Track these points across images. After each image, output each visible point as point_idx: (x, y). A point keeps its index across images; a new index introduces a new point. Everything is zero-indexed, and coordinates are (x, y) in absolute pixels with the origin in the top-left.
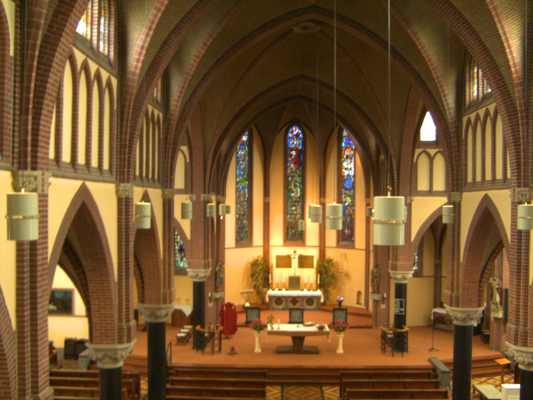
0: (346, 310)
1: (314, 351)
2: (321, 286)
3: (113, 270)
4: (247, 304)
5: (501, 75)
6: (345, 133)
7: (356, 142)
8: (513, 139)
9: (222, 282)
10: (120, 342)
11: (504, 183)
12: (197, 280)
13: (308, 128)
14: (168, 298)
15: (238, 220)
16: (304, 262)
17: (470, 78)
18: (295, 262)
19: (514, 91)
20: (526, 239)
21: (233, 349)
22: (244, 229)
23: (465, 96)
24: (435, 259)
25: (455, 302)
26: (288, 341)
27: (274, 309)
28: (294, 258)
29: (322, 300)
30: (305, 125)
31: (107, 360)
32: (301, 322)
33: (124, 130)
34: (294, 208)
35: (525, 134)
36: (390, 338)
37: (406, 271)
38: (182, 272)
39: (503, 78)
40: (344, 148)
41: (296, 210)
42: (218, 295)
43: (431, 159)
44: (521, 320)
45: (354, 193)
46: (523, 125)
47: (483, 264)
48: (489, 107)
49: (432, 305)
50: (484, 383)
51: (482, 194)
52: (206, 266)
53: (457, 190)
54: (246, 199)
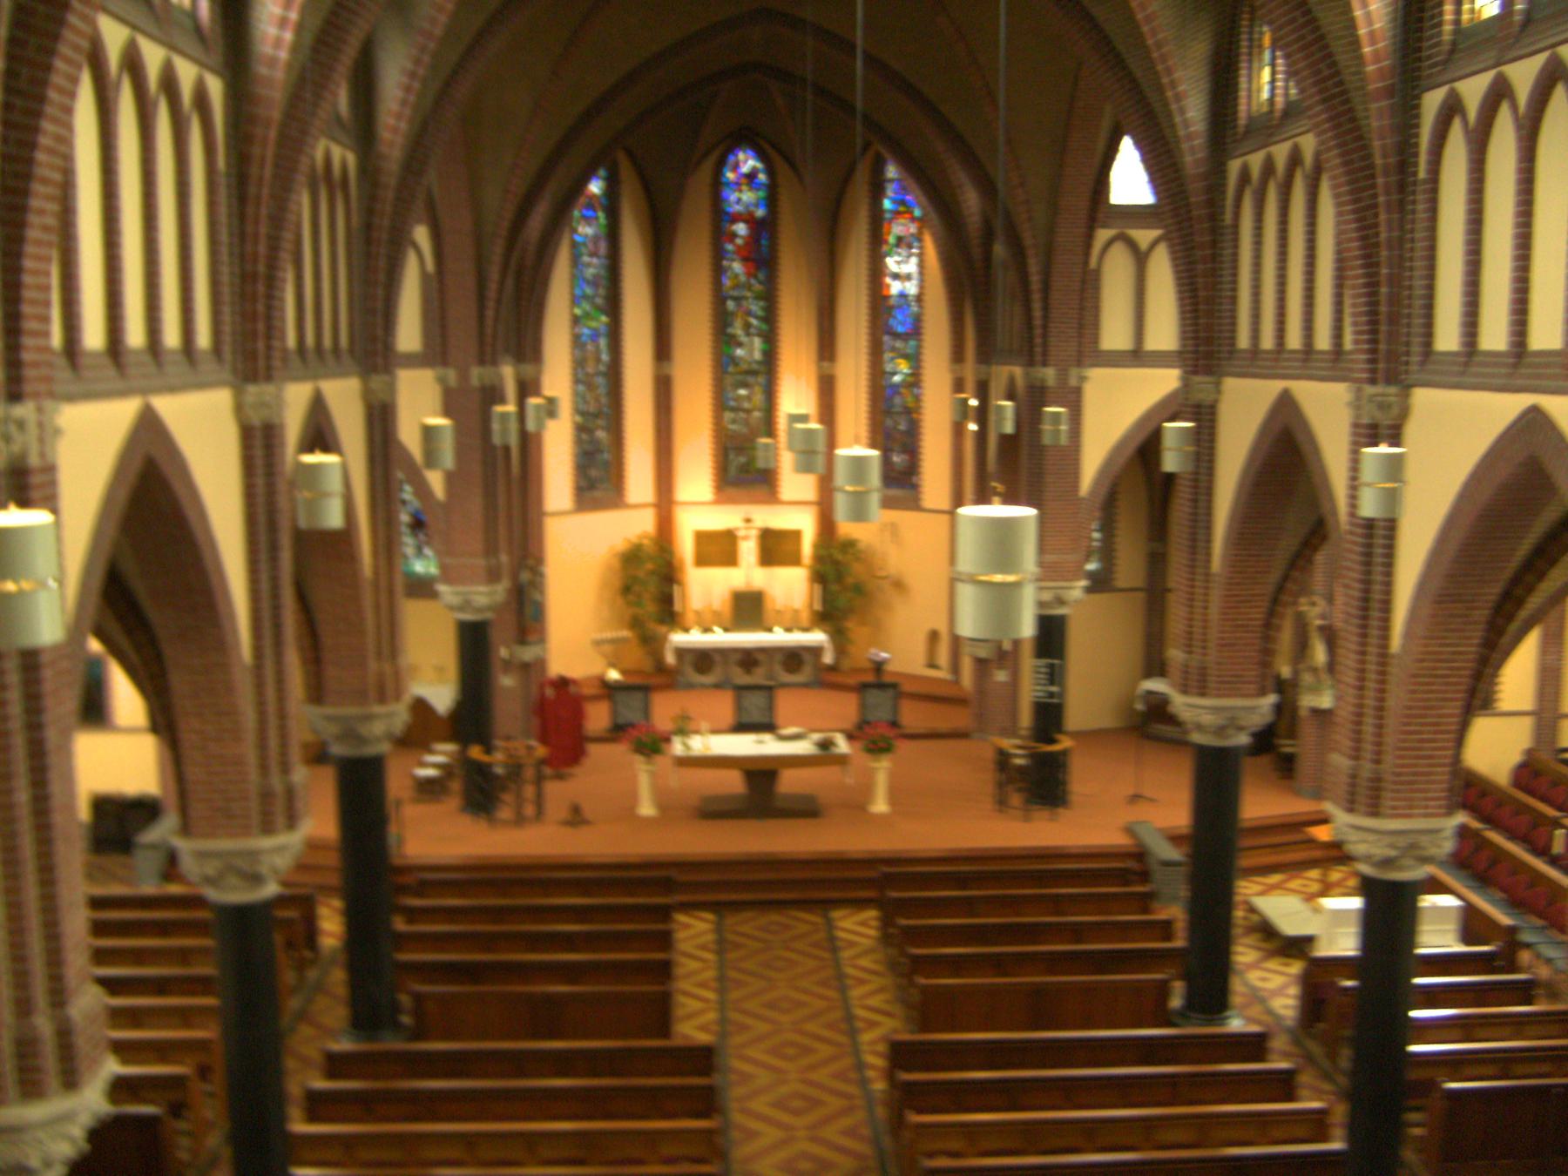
0: (894, 686)
1: (806, 809)
2: (827, 616)
3: (235, 631)
4: (614, 675)
5: (1334, 64)
6: (892, 171)
7: (923, 199)
8: (1361, 248)
9: (539, 613)
10: (268, 828)
11: (1333, 365)
12: (468, 617)
13: (780, 152)
14: (387, 689)
15: (582, 431)
16: (776, 548)
17: (1250, 47)
18: (748, 549)
19: (1366, 110)
20: (1385, 537)
21: (576, 809)
23: (1236, 99)
25: (1197, 683)
26: (734, 783)
27: (691, 686)
29: (828, 658)
30: (773, 146)
31: (233, 880)
32: (766, 726)
33: (250, 229)
34: (742, 392)
36: (1020, 769)
37: (1067, 580)
38: (422, 588)
39: (1338, 73)
40: (888, 216)
42: (528, 654)
43: (1141, 259)
44: (1368, 747)
45: (919, 347)
47: (1274, 577)
48: (1298, 139)
50: (1279, 891)
51: (1275, 387)
52: (493, 576)
53: (1209, 371)
54: (602, 368)
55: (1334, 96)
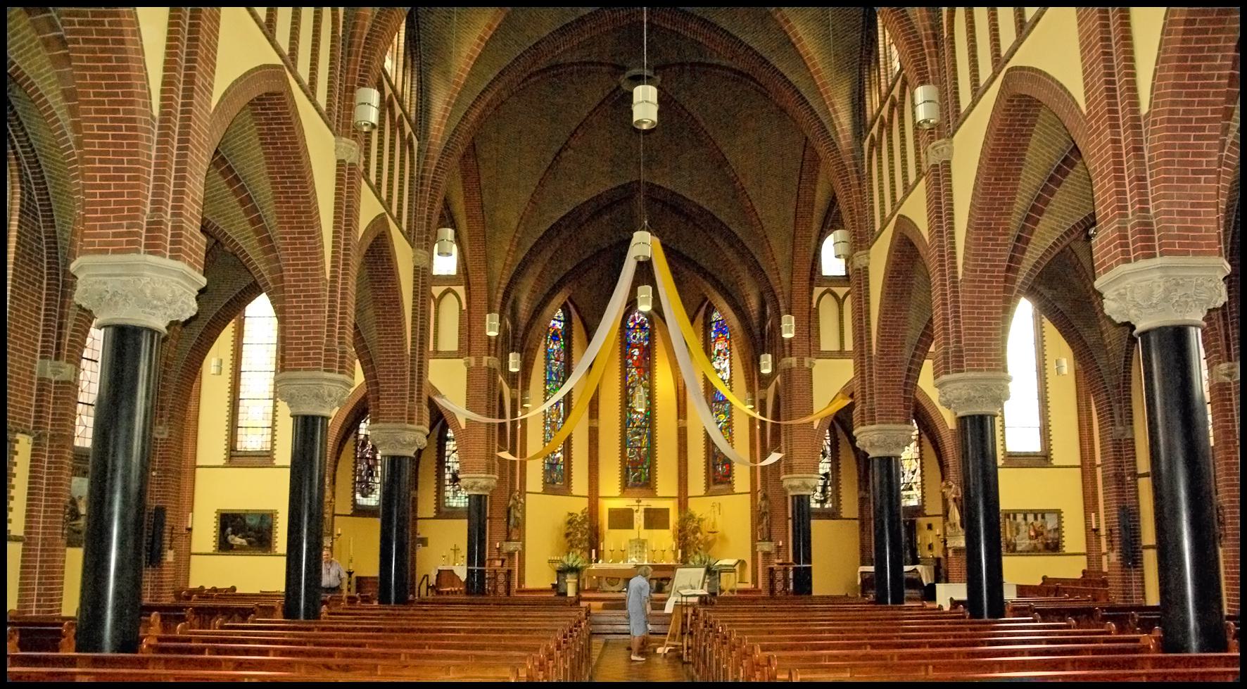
16: (655, 519)
18: (639, 519)
22: (558, 467)
24: (860, 488)
28: (637, 511)
35: (936, 67)
41: (640, 440)
46: (931, 56)
49: (859, 561)
55: (909, 34)
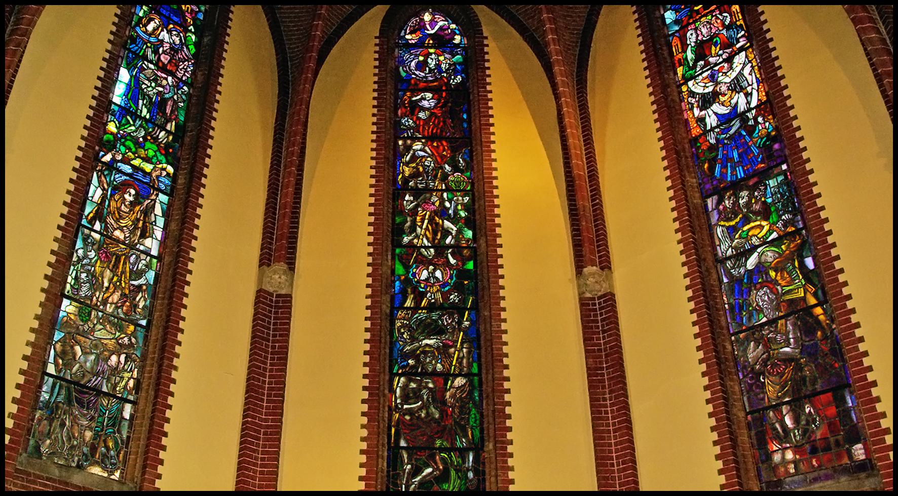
41: (443, 351)
